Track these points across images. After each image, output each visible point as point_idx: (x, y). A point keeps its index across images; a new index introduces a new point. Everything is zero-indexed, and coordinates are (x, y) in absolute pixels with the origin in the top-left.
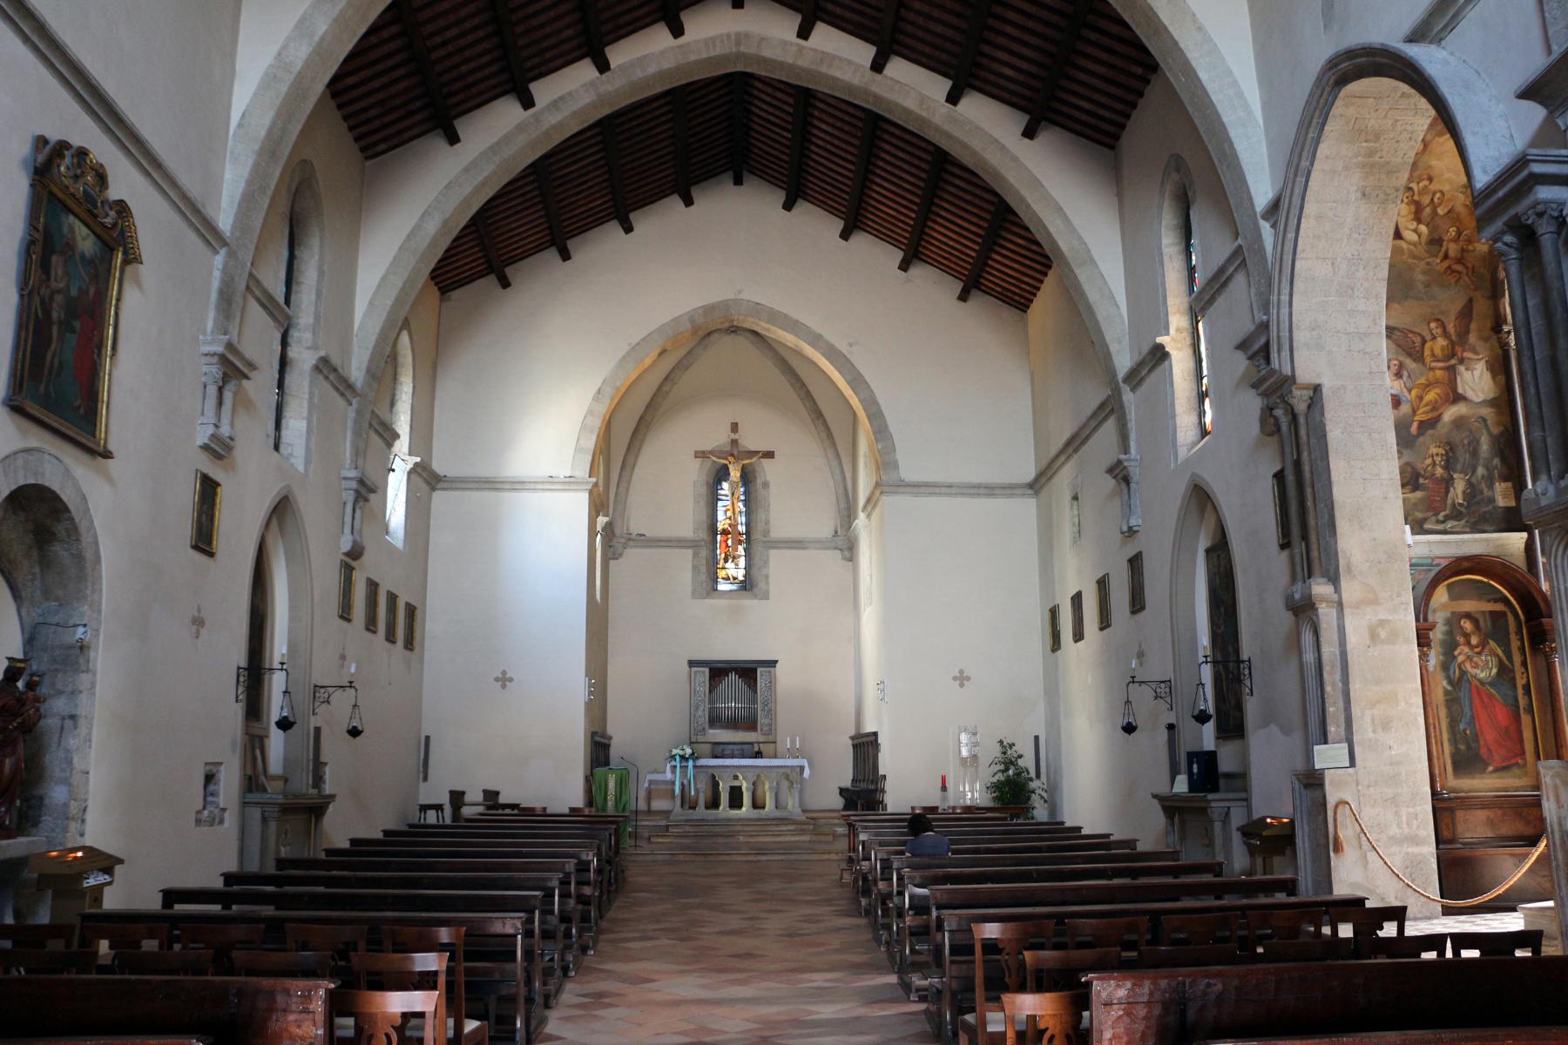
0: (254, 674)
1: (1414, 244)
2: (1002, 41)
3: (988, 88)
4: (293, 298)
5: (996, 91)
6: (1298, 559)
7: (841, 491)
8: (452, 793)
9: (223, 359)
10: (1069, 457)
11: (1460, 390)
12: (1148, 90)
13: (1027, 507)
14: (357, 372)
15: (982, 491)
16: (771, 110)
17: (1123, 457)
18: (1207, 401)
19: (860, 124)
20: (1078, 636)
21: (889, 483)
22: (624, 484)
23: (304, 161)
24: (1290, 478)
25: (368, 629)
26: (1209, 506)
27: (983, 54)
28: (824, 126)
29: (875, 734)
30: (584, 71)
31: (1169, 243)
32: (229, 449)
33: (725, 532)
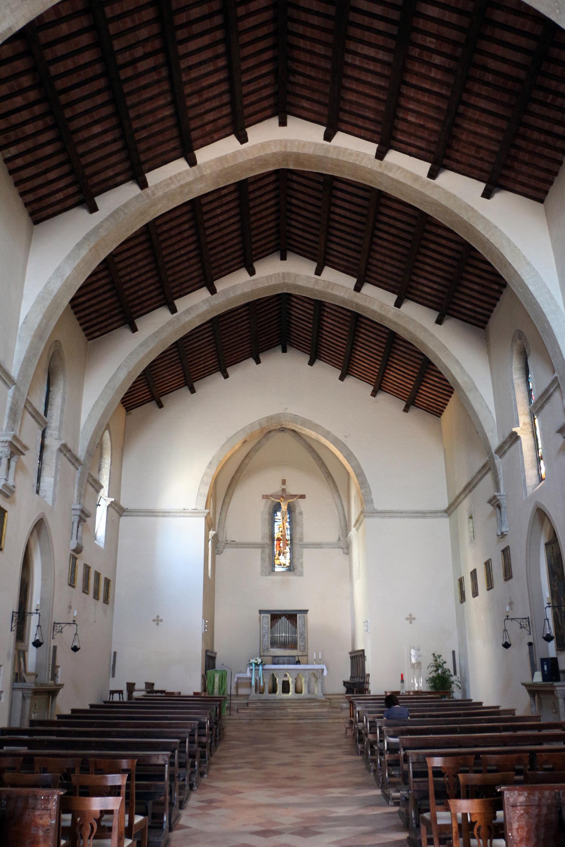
0: (21, 616)
3: (416, 298)
4: (49, 412)
5: (421, 300)
7: (342, 516)
8: (128, 684)
9: (11, 444)
10: (467, 495)
13: (445, 522)
14: (81, 452)
15: (419, 515)
18: (542, 462)
19: (349, 319)
20: (475, 594)
21: (369, 511)
22: (223, 516)
23: (56, 341)
25: (84, 592)
26: (546, 520)
27: (418, 261)
28: (329, 321)
29: (363, 651)
30: (203, 294)
32: (13, 492)
33: (279, 539)
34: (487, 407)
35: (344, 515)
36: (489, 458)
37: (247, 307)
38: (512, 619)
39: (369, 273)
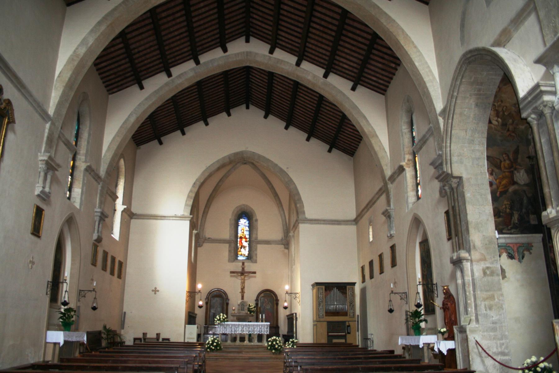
1: (496, 126)
4: (78, 143)
5: (342, 74)
6: (454, 244)
7: (284, 223)
11: (515, 180)
12: (397, 73)
13: (353, 229)
14: (102, 172)
15: (336, 223)
17: (388, 208)
18: (419, 187)
23: (84, 93)
24: (451, 212)
28: (279, 87)
31: (405, 128)
33: (241, 238)
35: (286, 222)
38: (395, 293)
39: (306, 54)
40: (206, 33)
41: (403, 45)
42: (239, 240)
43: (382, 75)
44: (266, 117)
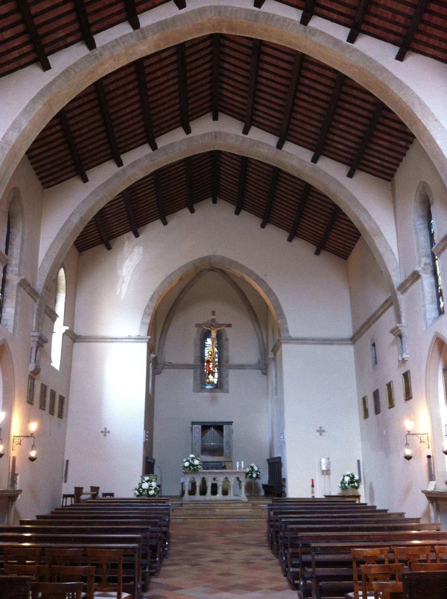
2: (338, 132)
5: (335, 157)
13: (350, 350)
14: (39, 286)
16: (229, 168)
17: (398, 325)
25: (41, 408)
28: (254, 176)
33: (208, 362)
34: (391, 250)
36: (392, 294)
37: (183, 163)
39: (290, 132)
40: (165, 109)
41: (420, 117)
42: (205, 364)
43: (389, 156)
44: (237, 213)
